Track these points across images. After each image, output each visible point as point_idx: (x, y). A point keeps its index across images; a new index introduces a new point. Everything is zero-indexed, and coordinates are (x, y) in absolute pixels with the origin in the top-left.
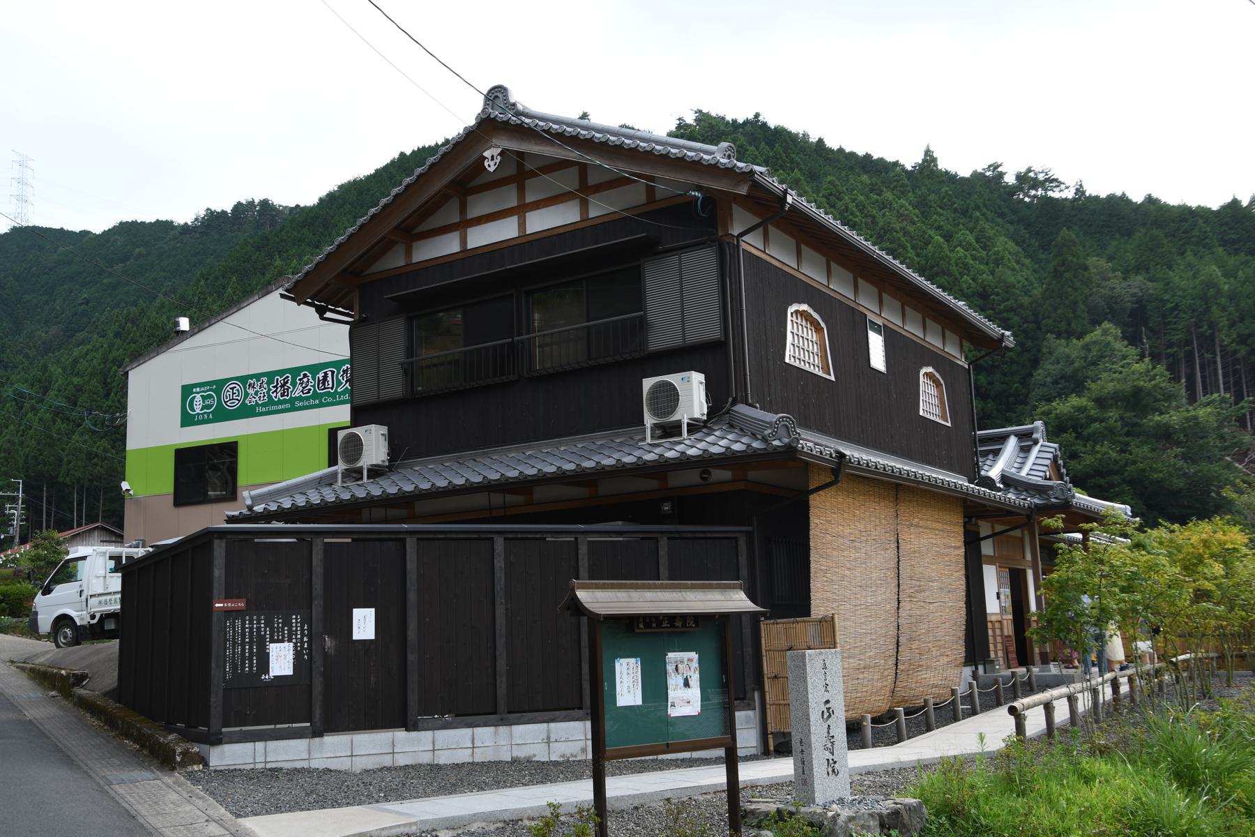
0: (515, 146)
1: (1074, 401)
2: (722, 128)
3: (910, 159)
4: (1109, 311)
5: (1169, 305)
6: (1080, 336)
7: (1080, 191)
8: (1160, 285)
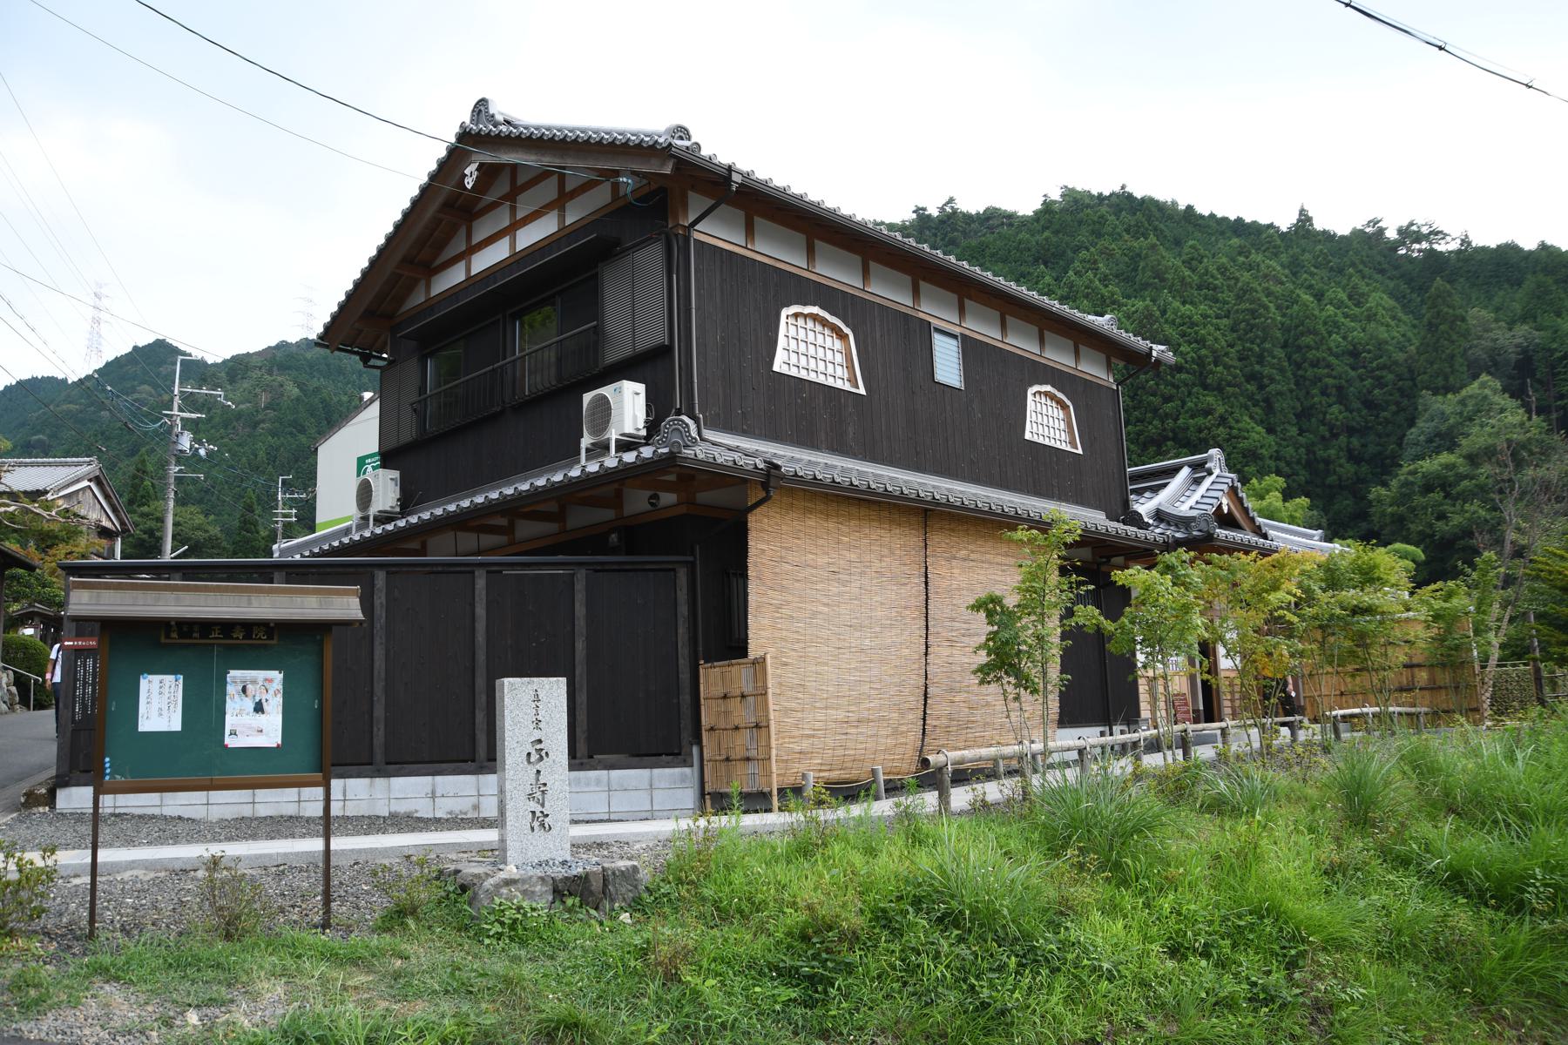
0: (488, 157)
1: (1445, 458)
2: (1087, 201)
3: (1285, 221)
4: (1493, 364)
5: (1558, 355)
6: (1456, 390)
7: (1465, 241)
8: (1548, 334)
